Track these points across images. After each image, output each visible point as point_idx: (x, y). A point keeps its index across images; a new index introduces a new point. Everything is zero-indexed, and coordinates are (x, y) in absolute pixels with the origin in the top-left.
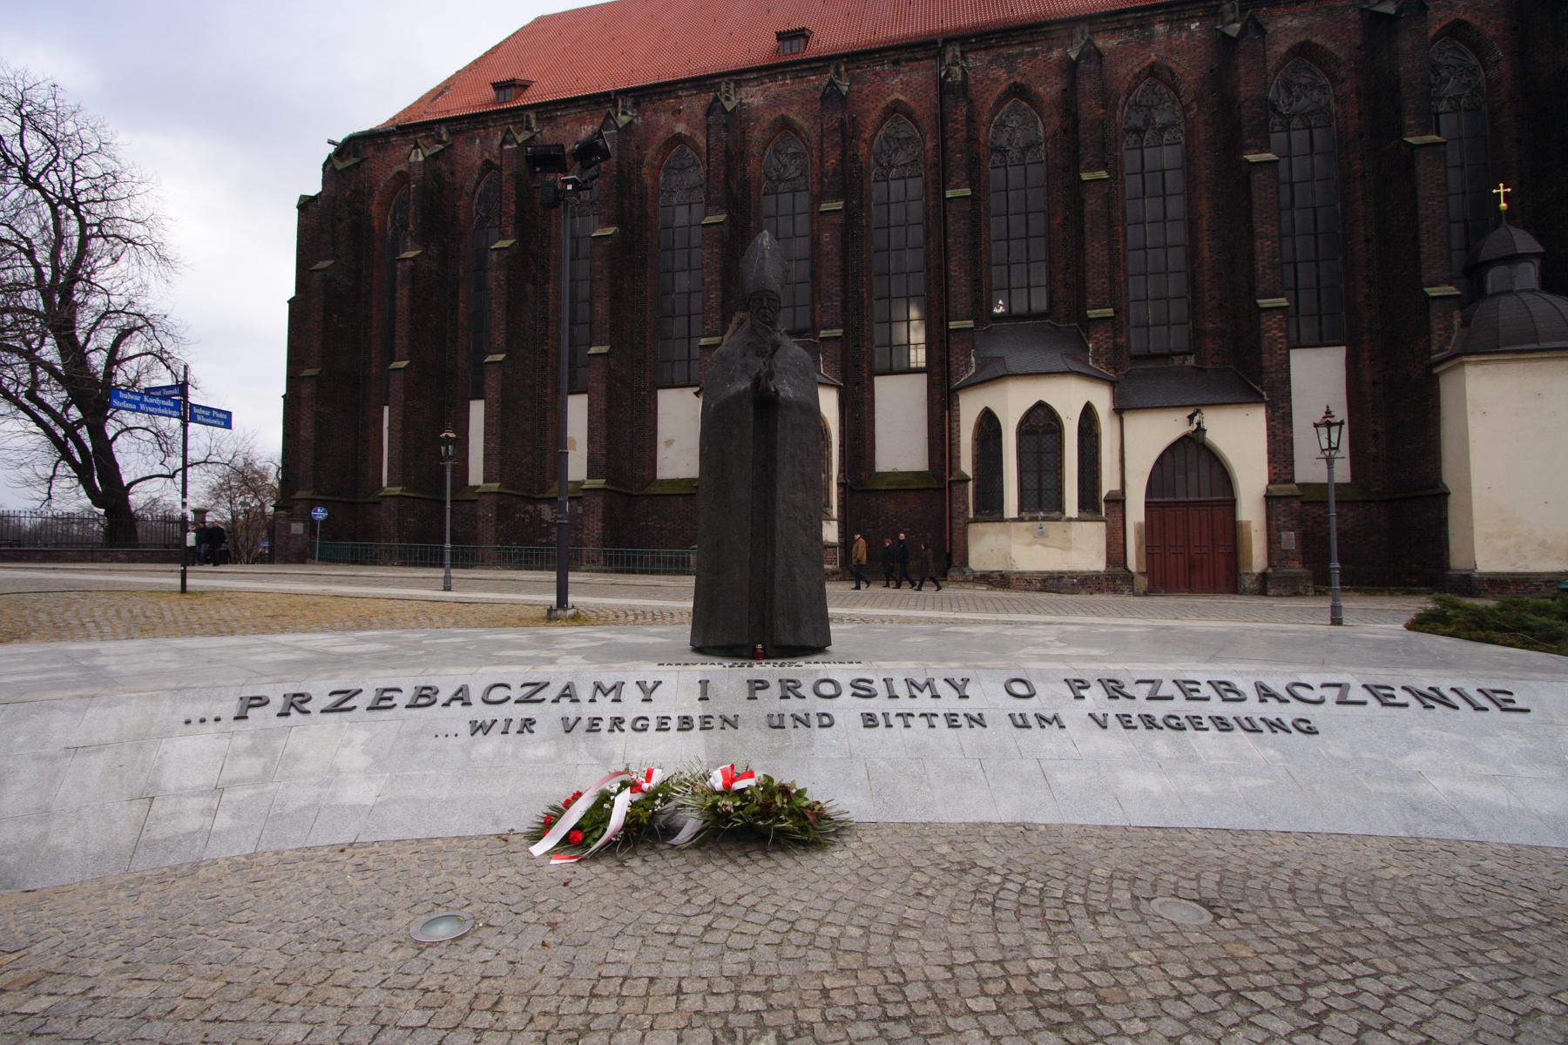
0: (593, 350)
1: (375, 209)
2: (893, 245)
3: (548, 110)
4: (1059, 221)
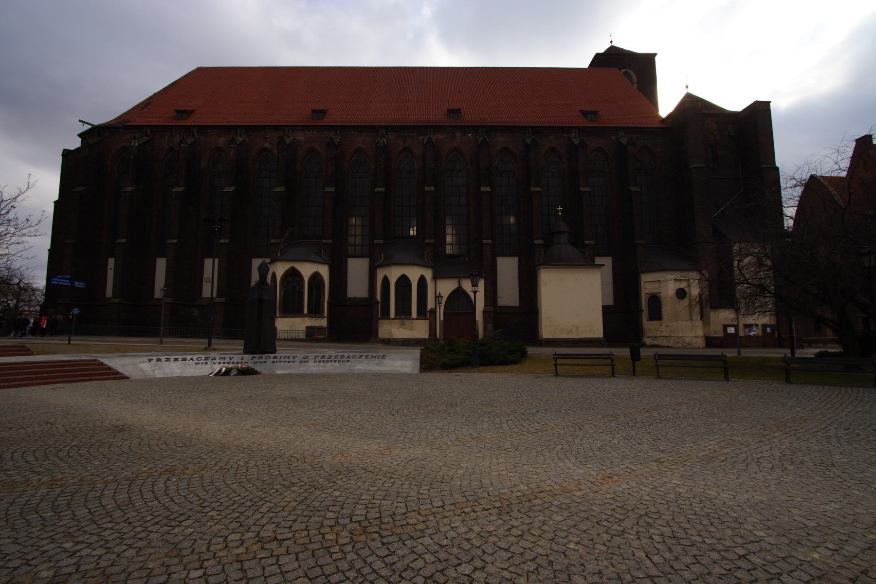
0: (222, 241)
3: (203, 129)
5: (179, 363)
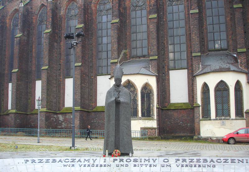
1: (8, 21)
2: (175, 27)
4: (229, 19)
5: (50, 164)
